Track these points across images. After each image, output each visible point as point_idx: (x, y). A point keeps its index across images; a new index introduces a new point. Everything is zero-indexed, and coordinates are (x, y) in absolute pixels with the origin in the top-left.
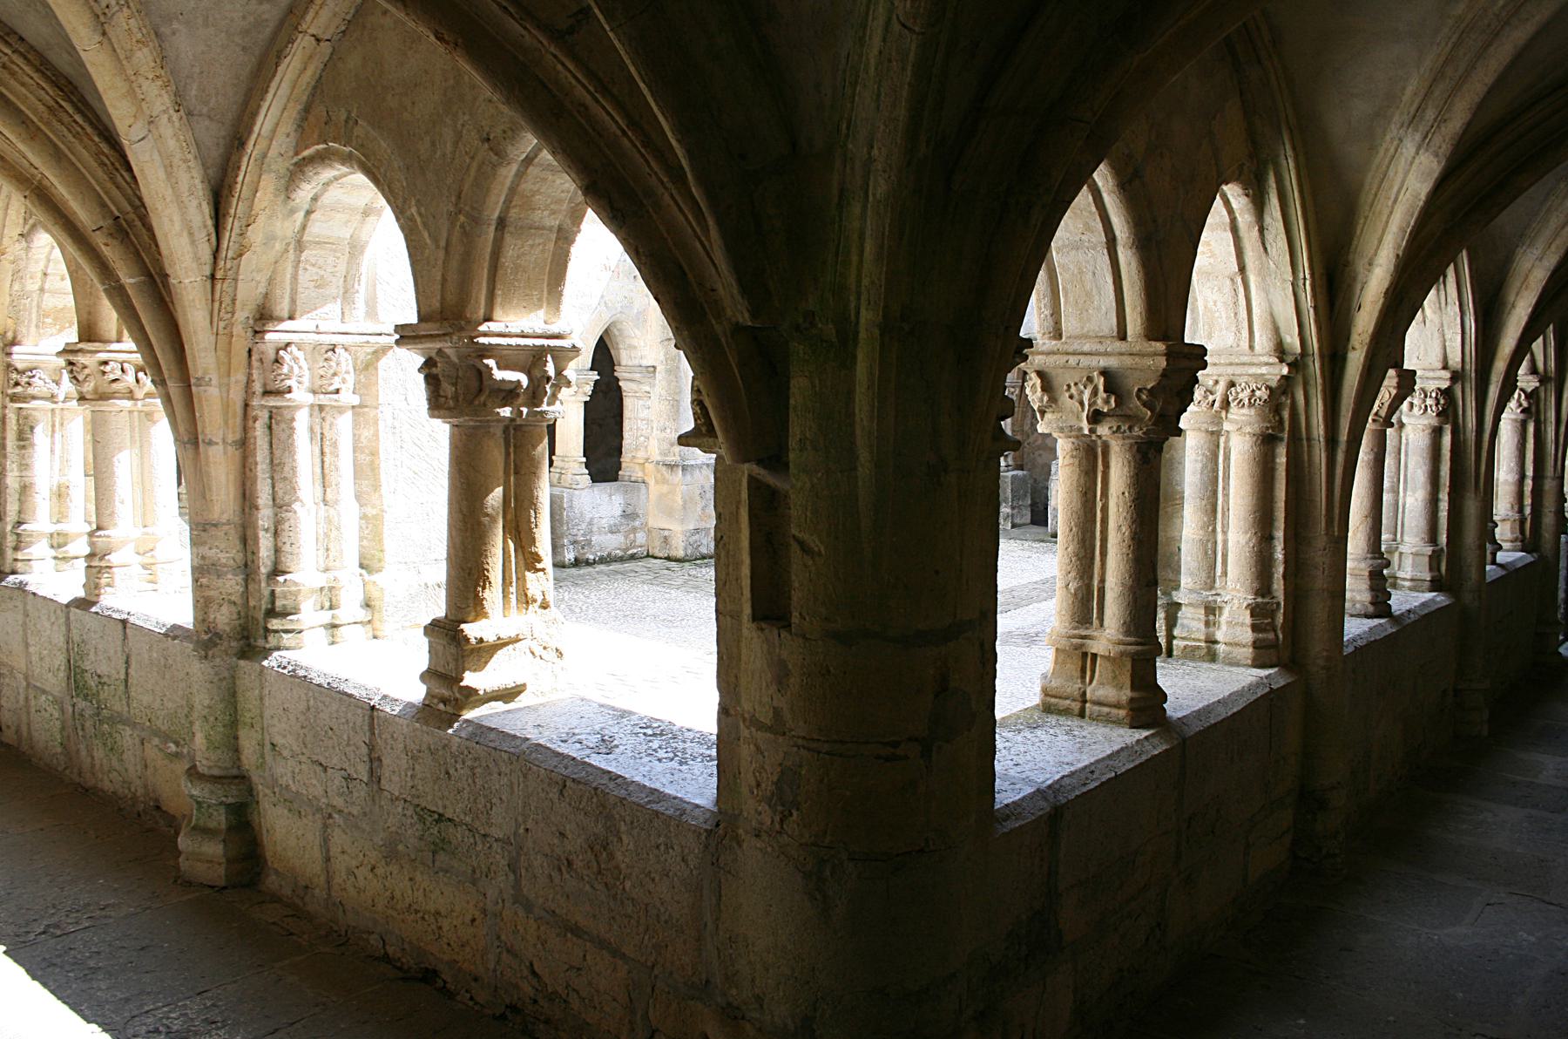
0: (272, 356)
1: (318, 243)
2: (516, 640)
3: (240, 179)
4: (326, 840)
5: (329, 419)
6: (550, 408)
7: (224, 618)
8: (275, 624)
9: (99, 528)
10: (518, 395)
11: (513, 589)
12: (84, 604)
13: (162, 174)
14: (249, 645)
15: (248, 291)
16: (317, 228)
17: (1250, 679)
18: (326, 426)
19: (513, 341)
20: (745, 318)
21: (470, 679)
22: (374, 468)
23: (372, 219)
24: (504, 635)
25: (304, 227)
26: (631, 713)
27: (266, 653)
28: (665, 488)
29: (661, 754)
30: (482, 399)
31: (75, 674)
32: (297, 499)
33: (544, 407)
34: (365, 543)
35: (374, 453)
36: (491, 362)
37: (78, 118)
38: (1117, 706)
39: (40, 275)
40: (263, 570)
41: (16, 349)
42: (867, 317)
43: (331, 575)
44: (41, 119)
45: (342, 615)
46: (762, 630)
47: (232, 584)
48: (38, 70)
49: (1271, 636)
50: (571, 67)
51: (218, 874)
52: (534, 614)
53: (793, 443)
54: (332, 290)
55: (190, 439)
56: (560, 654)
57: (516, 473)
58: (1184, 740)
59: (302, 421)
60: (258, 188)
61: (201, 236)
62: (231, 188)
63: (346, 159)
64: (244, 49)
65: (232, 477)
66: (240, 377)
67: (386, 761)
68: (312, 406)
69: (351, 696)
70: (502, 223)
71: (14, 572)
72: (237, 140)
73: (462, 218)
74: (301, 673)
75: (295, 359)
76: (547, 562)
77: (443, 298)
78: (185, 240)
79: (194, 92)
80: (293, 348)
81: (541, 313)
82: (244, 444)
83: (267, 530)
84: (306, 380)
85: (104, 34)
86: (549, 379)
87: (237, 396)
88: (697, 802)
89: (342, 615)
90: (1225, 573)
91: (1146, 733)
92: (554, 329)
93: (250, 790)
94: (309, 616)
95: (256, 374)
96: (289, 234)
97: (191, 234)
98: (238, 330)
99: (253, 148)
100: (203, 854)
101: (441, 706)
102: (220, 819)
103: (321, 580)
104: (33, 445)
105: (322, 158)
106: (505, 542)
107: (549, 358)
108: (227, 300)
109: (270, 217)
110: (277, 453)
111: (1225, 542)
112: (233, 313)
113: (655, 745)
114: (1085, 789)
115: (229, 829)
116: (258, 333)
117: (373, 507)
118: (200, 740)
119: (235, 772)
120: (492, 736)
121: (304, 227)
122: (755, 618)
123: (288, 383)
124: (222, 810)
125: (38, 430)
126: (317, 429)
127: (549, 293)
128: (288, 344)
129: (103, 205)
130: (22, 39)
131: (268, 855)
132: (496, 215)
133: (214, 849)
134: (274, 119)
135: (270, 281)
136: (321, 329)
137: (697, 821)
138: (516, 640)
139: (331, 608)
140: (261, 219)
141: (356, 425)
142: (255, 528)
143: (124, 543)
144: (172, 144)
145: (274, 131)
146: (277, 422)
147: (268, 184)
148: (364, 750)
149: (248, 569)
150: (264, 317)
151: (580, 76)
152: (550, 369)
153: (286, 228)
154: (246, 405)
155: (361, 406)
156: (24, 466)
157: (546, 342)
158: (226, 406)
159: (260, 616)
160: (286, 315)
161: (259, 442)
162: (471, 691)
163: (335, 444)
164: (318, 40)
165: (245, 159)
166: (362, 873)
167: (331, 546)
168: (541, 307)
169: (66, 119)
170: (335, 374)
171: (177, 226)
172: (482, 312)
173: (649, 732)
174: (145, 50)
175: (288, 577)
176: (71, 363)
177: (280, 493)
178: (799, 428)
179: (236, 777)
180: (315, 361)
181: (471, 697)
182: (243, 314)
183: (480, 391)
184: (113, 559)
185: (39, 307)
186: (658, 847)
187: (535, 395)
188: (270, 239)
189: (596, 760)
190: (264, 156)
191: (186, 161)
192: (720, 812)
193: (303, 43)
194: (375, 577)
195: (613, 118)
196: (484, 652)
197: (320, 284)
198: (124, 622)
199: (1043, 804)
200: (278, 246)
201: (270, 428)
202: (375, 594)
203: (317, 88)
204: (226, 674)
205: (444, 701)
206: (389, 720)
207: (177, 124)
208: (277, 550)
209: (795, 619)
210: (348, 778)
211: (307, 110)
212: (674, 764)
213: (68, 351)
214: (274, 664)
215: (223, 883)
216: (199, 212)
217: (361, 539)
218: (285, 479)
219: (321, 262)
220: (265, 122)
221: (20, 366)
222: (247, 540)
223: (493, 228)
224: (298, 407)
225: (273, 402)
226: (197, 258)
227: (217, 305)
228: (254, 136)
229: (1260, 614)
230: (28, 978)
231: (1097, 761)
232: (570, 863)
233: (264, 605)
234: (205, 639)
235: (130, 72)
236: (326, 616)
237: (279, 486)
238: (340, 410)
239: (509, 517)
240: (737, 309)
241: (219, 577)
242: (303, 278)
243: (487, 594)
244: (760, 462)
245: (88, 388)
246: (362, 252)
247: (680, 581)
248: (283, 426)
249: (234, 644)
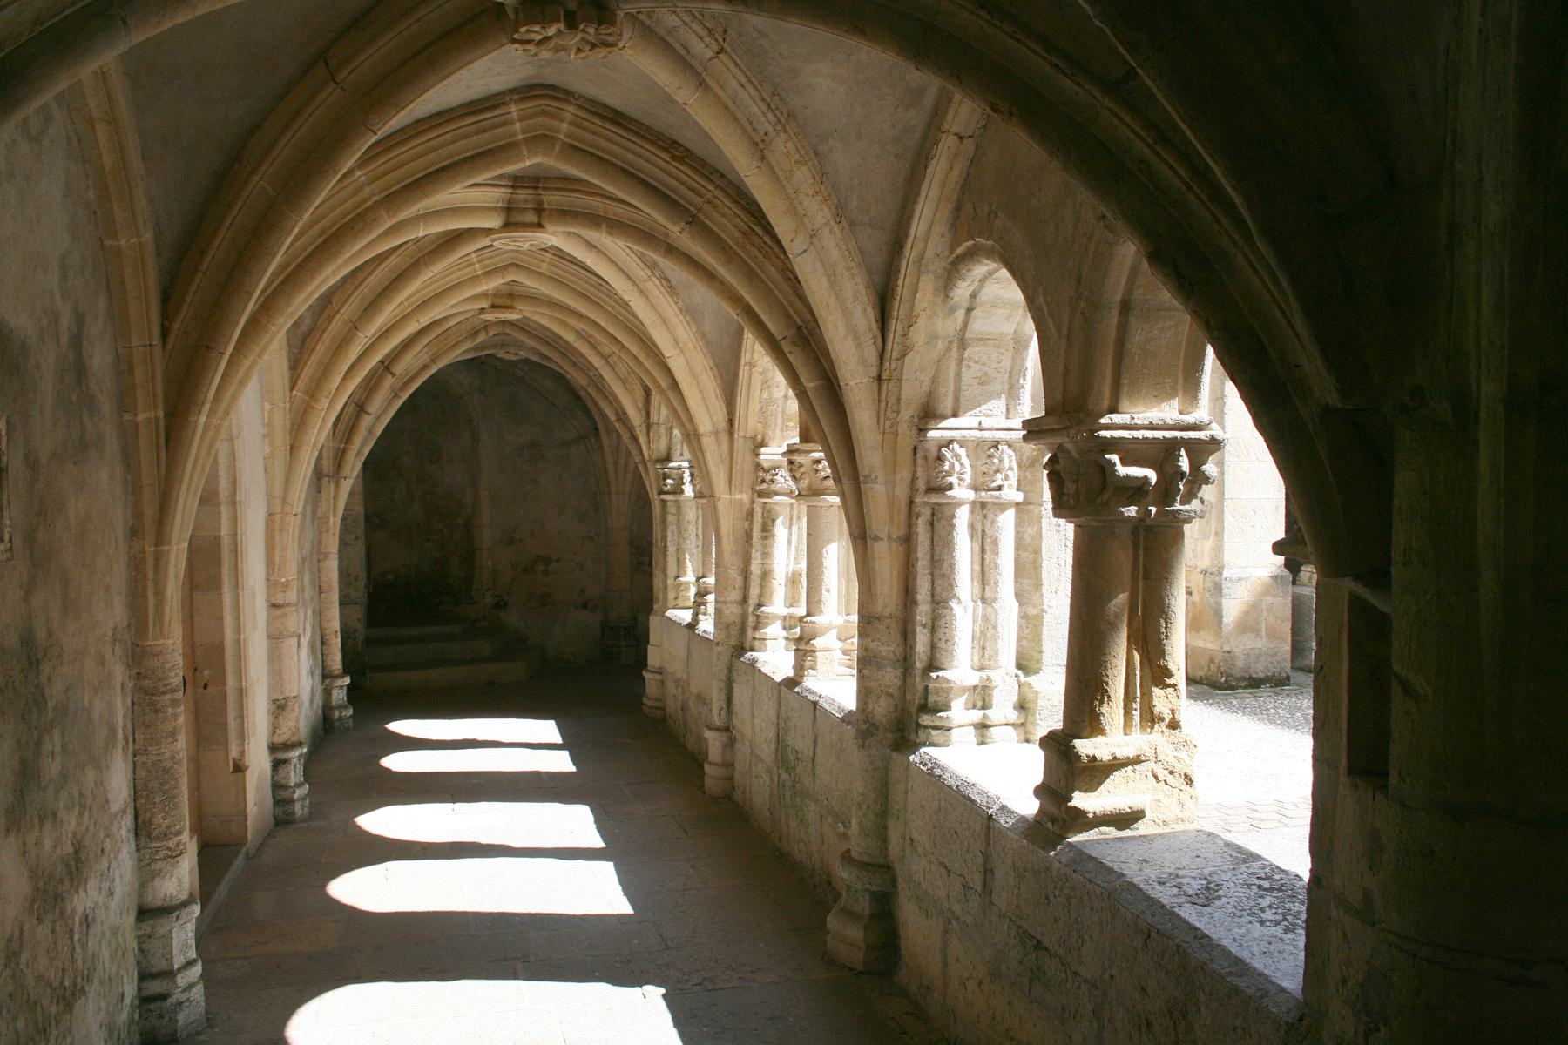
0: (933, 452)
1: (980, 340)
2: (1136, 761)
3: (900, 282)
4: (945, 945)
5: (990, 516)
6: (1187, 507)
7: (881, 709)
8: (926, 719)
9: (808, 614)
10: (1147, 492)
11: (1137, 705)
12: (791, 683)
13: (824, 282)
14: (903, 738)
15: (912, 390)
16: (979, 325)
18: (988, 523)
19: (1139, 434)
20: (1333, 399)
21: (1080, 800)
22: (1037, 567)
24: (1122, 753)
25: (965, 325)
26: (1258, 857)
27: (915, 747)
29: (1269, 915)
30: (1105, 497)
31: (781, 744)
32: (955, 596)
33: (1178, 507)
34: (1024, 643)
35: (1037, 552)
36: (1114, 458)
40: (919, 665)
41: (763, 450)
42: (1489, 391)
43: (984, 674)
44: (737, 243)
45: (994, 715)
46: (1357, 787)
47: (890, 677)
48: (735, 201)
50: (1128, 119)
51: (857, 958)
52: (1158, 738)
53: (1396, 555)
54: (996, 386)
55: (861, 538)
56: (1189, 780)
57: (1146, 578)
59: (962, 517)
62: (893, 291)
63: (990, 254)
64: (896, 156)
65: (895, 572)
66: (904, 474)
67: (997, 875)
68: (973, 503)
69: (973, 802)
70: (1126, 307)
71: (752, 650)
72: (896, 246)
73: (1082, 304)
74: (938, 772)
75: (957, 457)
76: (1179, 678)
77: (1065, 389)
79: (855, 203)
80: (956, 446)
81: (1175, 403)
82: (908, 540)
83: (924, 626)
84: (968, 478)
85: (763, 158)
86: (1183, 474)
87: (901, 492)
89: (994, 715)
92: (1190, 419)
93: (894, 882)
94: (960, 713)
95: (919, 474)
96: (952, 332)
97: (856, 338)
98: (903, 428)
99: (910, 251)
100: (847, 935)
101: (1049, 825)
102: (864, 905)
103: (973, 679)
104: (773, 536)
105: (971, 255)
106: (1129, 653)
107: (1183, 452)
108: (893, 400)
109: (931, 317)
110: (938, 550)
112: (898, 412)
113: (1265, 902)
115: (872, 915)
116: (922, 431)
117: (1034, 606)
118: (854, 829)
119: (881, 861)
120: (1090, 866)
121: (965, 325)
122: (1351, 771)
123: (950, 479)
124: (868, 897)
125: (779, 522)
126: (979, 527)
127: (1185, 380)
128: (951, 442)
129: (788, 316)
130: (722, 176)
131: (903, 947)
132: (1118, 297)
133: (855, 933)
134: (928, 221)
135: (934, 380)
136: (984, 425)
138: (1136, 761)
139: (983, 707)
140: (922, 320)
141: (1020, 523)
142: (913, 622)
143: (828, 629)
144: (835, 254)
145: (928, 232)
146: (940, 520)
147: (927, 285)
148: (980, 860)
149: (906, 662)
150: (928, 414)
151: (1138, 129)
152: (1184, 464)
153: (948, 326)
154: (911, 502)
155: (1026, 502)
156: (766, 554)
157: (1178, 434)
158: (892, 502)
159: (914, 710)
160: (949, 411)
161: (921, 539)
162: (1079, 813)
163: (995, 542)
164: (961, 138)
166: (971, 985)
167: (988, 645)
168: (1172, 396)
169: (757, 241)
170: (998, 471)
171: (842, 331)
172: (1106, 403)
173: (1266, 884)
174: (804, 169)
175: (941, 673)
176: (791, 462)
177: (938, 589)
178: (1404, 535)
179: (882, 866)
180: (978, 458)
181: (1081, 820)
182: (907, 413)
183: (1104, 488)
184: (818, 643)
185: (783, 412)
186: (1235, 1029)
187: (1166, 491)
188: (932, 338)
189: (1189, 913)
190: (921, 257)
191: (849, 269)
193: (947, 143)
194: (1030, 679)
195: (1175, 171)
196: (1097, 772)
197: (984, 381)
198: (815, 704)
200: (941, 345)
201: (932, 524)
202: (1030, 696)
203: (966, 185)
204: (879, 764)
205: (1053, 820)
206: (1002, 832)
207: (839, 235)
208: (933, 647)
209: (1393, 780)
210: (966, 886)
211: (958, 208)
212: (1278, 930)
213: (791, 451)
214: (917, 760)
215: (860, 967)
216: (864, 316)
217: (1019, 639)
218: (943, 575)
219: (984, 358)
220: (918, 226)
221: (766, 465)
222: (907, 635)
223: (1115, 312)
224: (959, 504)
225: (935, 499)
226: (863, 361)
227: (883, 405)
228: (910, 239)
230: (671, 1024)
232: (1149, 1025)
233: (917, 700)
234: (862, 723)
235: (791, 191)
236: (976, 716)
237: (938, 582)
238: (1003, 507)
239: (1135, 626)
240: (1324, 388)
242: (967, 375)
243: (1105, 709)
244: (1358, 577)
245: (804, 483)
248: (944, 522)
249: (889, 736)
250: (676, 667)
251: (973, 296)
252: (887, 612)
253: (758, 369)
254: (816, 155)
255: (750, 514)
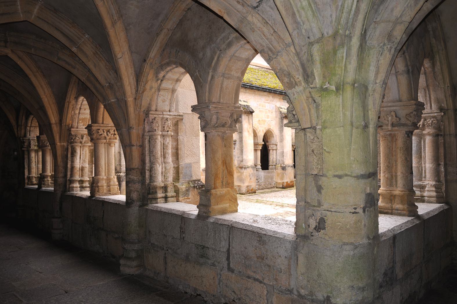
0: (151, 121)
15: (144, 103)
17: (439, 206)
23: (178, 82)
28: (239, 174)
29: (273, 223)
37: (101, 56)
38: (403, 210)
39: (79, 109)
41: (72, 129)
45: (169, 194)
49: (442, 194)
58: (424, 220)
60: (149, 74)
61: (133, 87)
78: (129, 87)
82: (142, 146)
83: (148, 170)
87: (141, 133)
88: (289, 233)
90: (425, 176)
91: (413, 218)
101: (204, 214)
105: (168, 64)
108: (139, 105)
111: (425, 167)
112: (141, 109)
114: (401, 231)
121: (160, 85)
135: (151, 100)
137: (290, 238)
139: (165, 193)
140: (149, 82)
144: (127, 60)
147: (73, 97)
149: (143, 182)
156: (73, 162)
164: (168, 30)
165: (146, 65)
171: (128, 83)
177: (152, 159)
185: (78, 118)
189: (254, 225)
192: (297, 235)
199: (391, 234)
218: (154, 155)
226: (132, 93)
229: (438, 188)
231: (402, 224)
236: (163, 195)
241: (134, 184)
246: (175, 92)
247: (245, 199)
248: (153, 140)
250: (285, 104)
251: (164, 77)
252: (136, 167)
253: (72, 104)
254: (127, 30)
255: (67, 149)
